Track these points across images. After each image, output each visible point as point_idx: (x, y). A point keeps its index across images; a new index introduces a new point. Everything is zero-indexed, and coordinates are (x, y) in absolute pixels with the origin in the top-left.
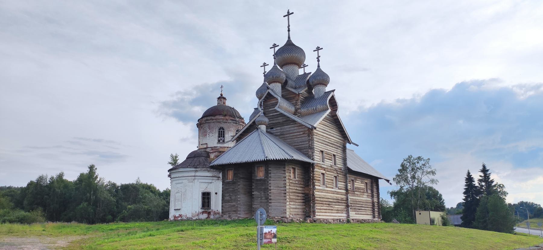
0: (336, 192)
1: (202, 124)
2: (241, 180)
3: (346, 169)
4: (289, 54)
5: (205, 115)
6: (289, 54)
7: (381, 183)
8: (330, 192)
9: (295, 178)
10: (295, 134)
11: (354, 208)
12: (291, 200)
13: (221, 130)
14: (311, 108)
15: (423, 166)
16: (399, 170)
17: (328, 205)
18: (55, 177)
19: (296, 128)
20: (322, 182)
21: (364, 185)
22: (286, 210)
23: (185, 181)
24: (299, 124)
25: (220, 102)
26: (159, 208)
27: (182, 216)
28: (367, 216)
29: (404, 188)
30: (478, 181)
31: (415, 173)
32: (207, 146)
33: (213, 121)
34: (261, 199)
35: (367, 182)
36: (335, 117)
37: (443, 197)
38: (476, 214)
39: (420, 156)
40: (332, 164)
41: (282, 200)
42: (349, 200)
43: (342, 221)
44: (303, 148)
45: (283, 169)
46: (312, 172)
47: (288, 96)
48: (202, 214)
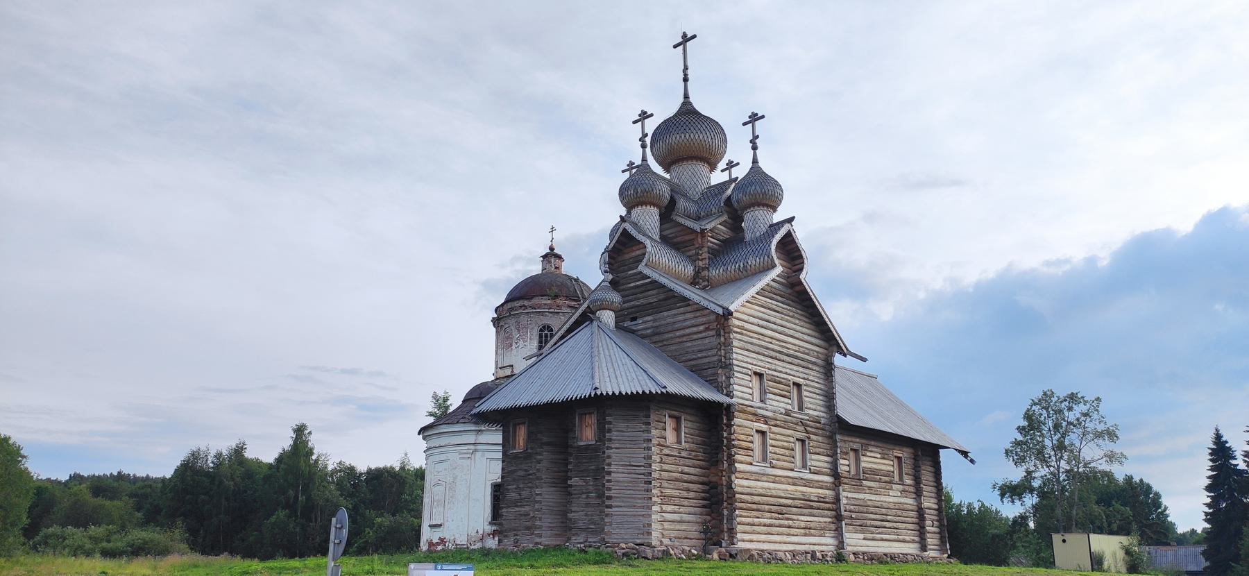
0: (804, 482)
1: (501, 318)
2: (546, 448)
3: (833, 421)
4: (683, 136)
5: (510, 298)
6: (683, 136)
7: (947, 459)
8: (783, 479)
9: (679, 442)
10: (688, 331)
11: (859, 522)
12: (666, 500)
13: (546, 332)
14: (733, 267)
15: (1083, 418)
16: (1018, 428)
17: (777, 515)
18: (225, 452)
19: (688, 316)
20: (757, 452)
21: (892, 463)
22: (650, 525)
23: (454, 457)
24: (695, 306)
25: (548, 266)
26: (1024, 544)
27: (446, 542)
28: (902, 545)
29: (1036, 475)
30: (1245, 456)
31: (1063, 436)
32: (512, 372)
33: (526, 311)
34: (588, 497)
35: (901, 455)
36: (798, 288)
37: (1165, 501)
38: (1242, 545)
39: (1075, 392)
40: (789, 407)
41: (639, 499)
42: (844, 501)
43: (821, 558)
44: (706, 367)
45: (645, 420)
46: (728, 427)
47: (679, 239)
48: (491, 536)
